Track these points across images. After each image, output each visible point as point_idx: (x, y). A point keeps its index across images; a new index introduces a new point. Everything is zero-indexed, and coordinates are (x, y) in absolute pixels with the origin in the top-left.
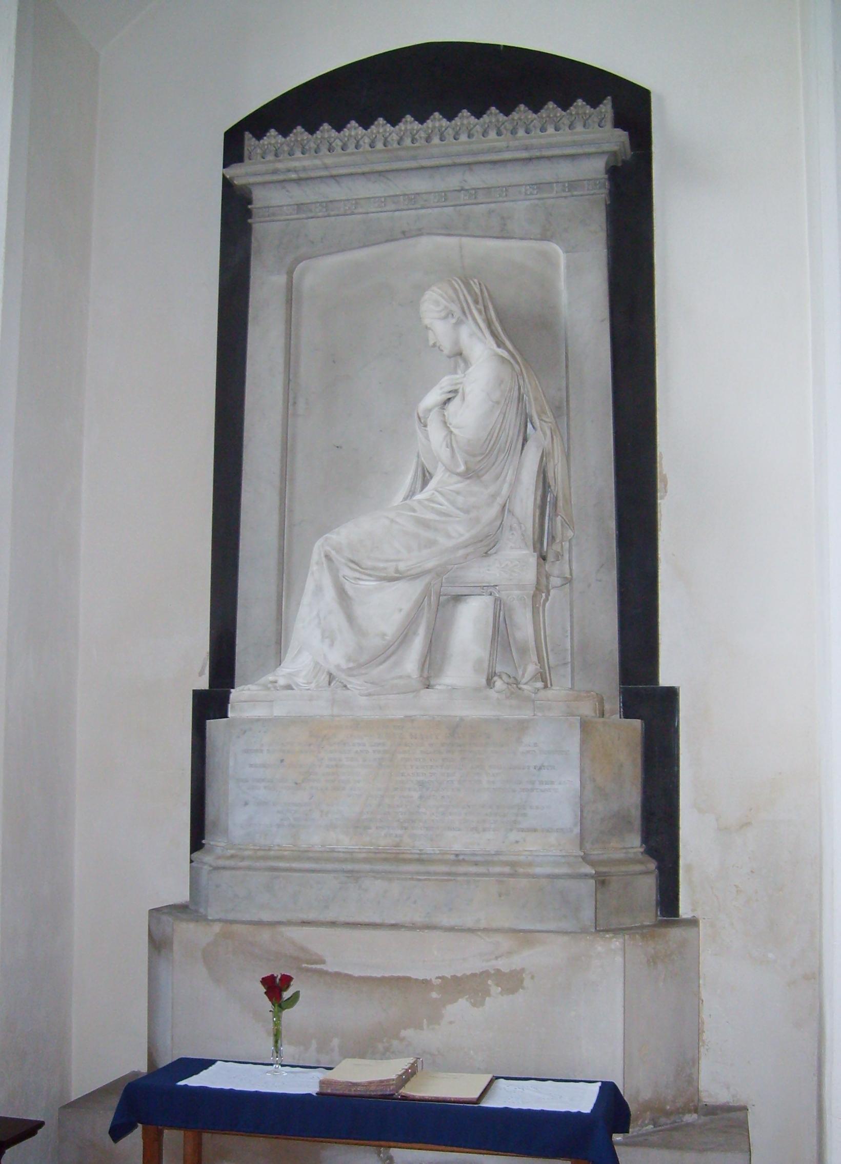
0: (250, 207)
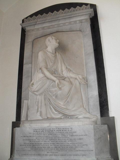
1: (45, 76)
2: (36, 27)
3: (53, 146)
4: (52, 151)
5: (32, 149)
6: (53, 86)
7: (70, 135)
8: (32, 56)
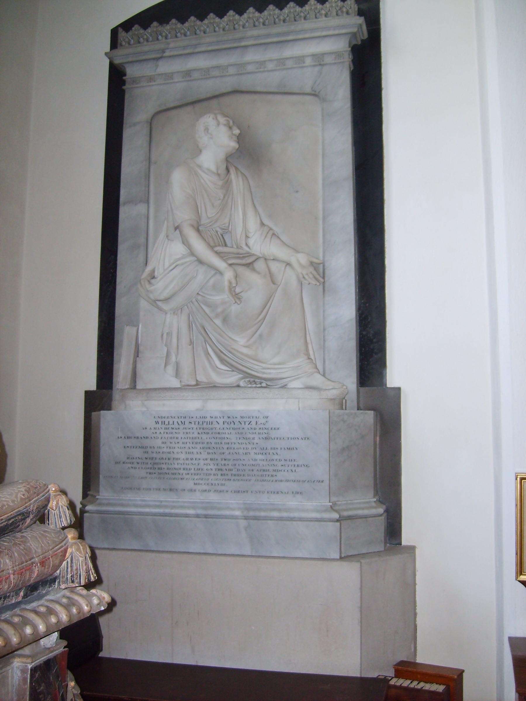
0: (124, 78)
1: (192, 253)
2: (164, 67)
3: (212, 466)
4: (208, 479)
5: (150, 473)
6: (217, 288)
7: (261, 436)
8: (148, 177)
